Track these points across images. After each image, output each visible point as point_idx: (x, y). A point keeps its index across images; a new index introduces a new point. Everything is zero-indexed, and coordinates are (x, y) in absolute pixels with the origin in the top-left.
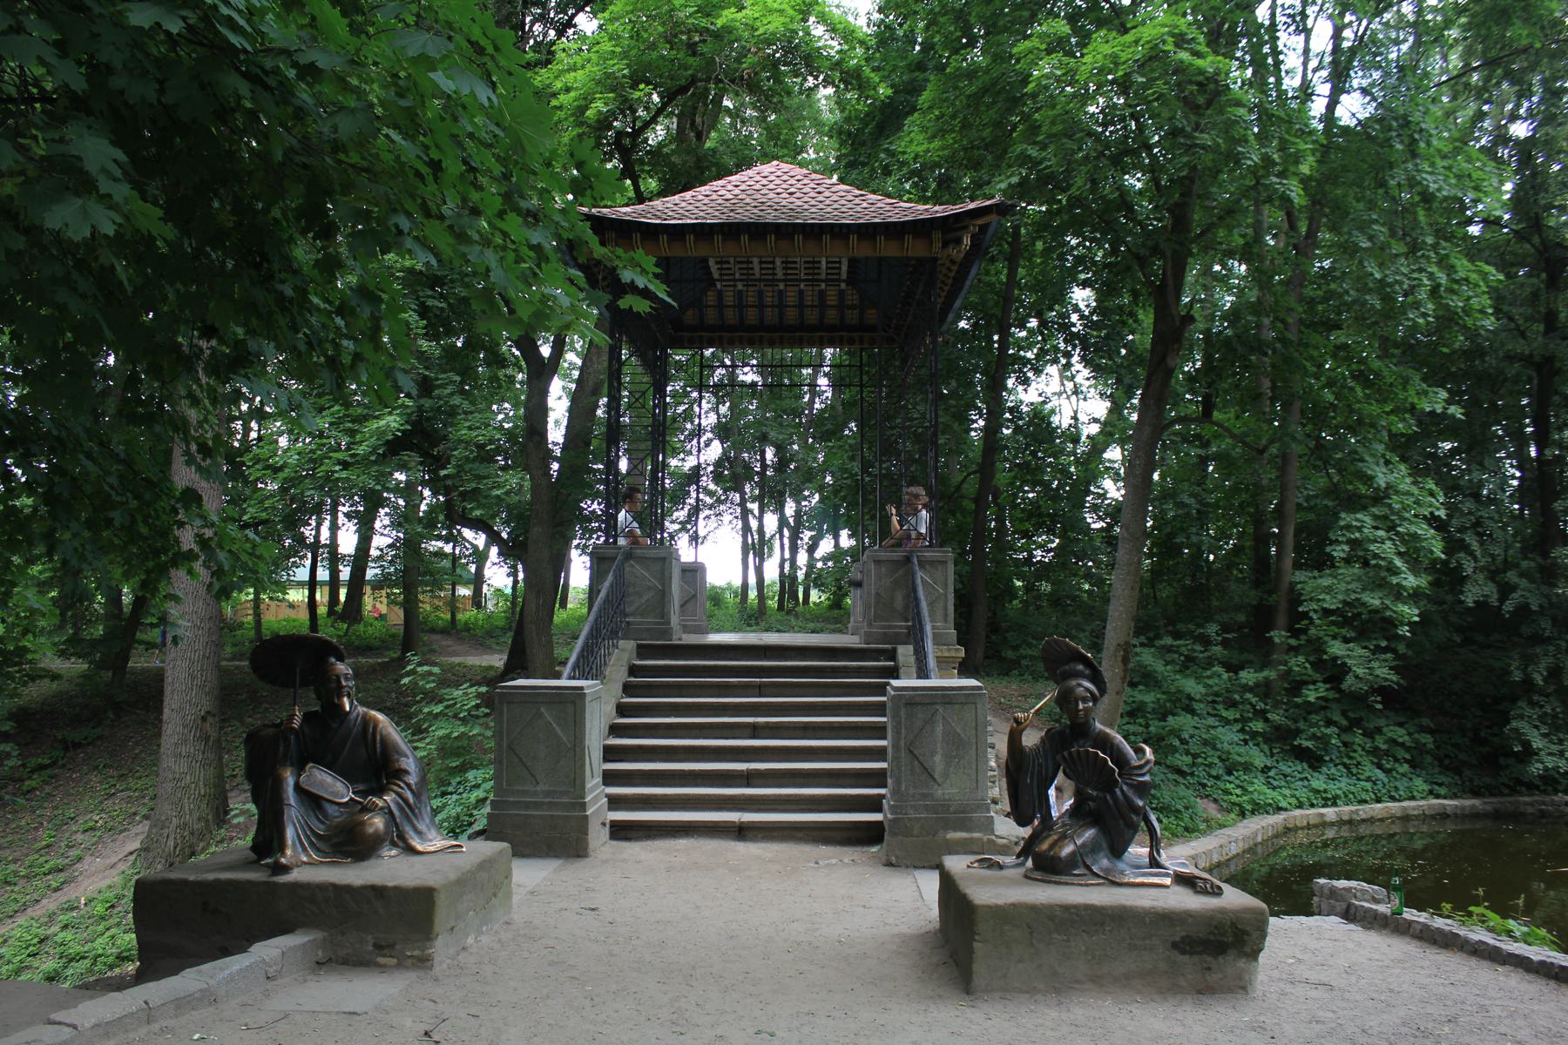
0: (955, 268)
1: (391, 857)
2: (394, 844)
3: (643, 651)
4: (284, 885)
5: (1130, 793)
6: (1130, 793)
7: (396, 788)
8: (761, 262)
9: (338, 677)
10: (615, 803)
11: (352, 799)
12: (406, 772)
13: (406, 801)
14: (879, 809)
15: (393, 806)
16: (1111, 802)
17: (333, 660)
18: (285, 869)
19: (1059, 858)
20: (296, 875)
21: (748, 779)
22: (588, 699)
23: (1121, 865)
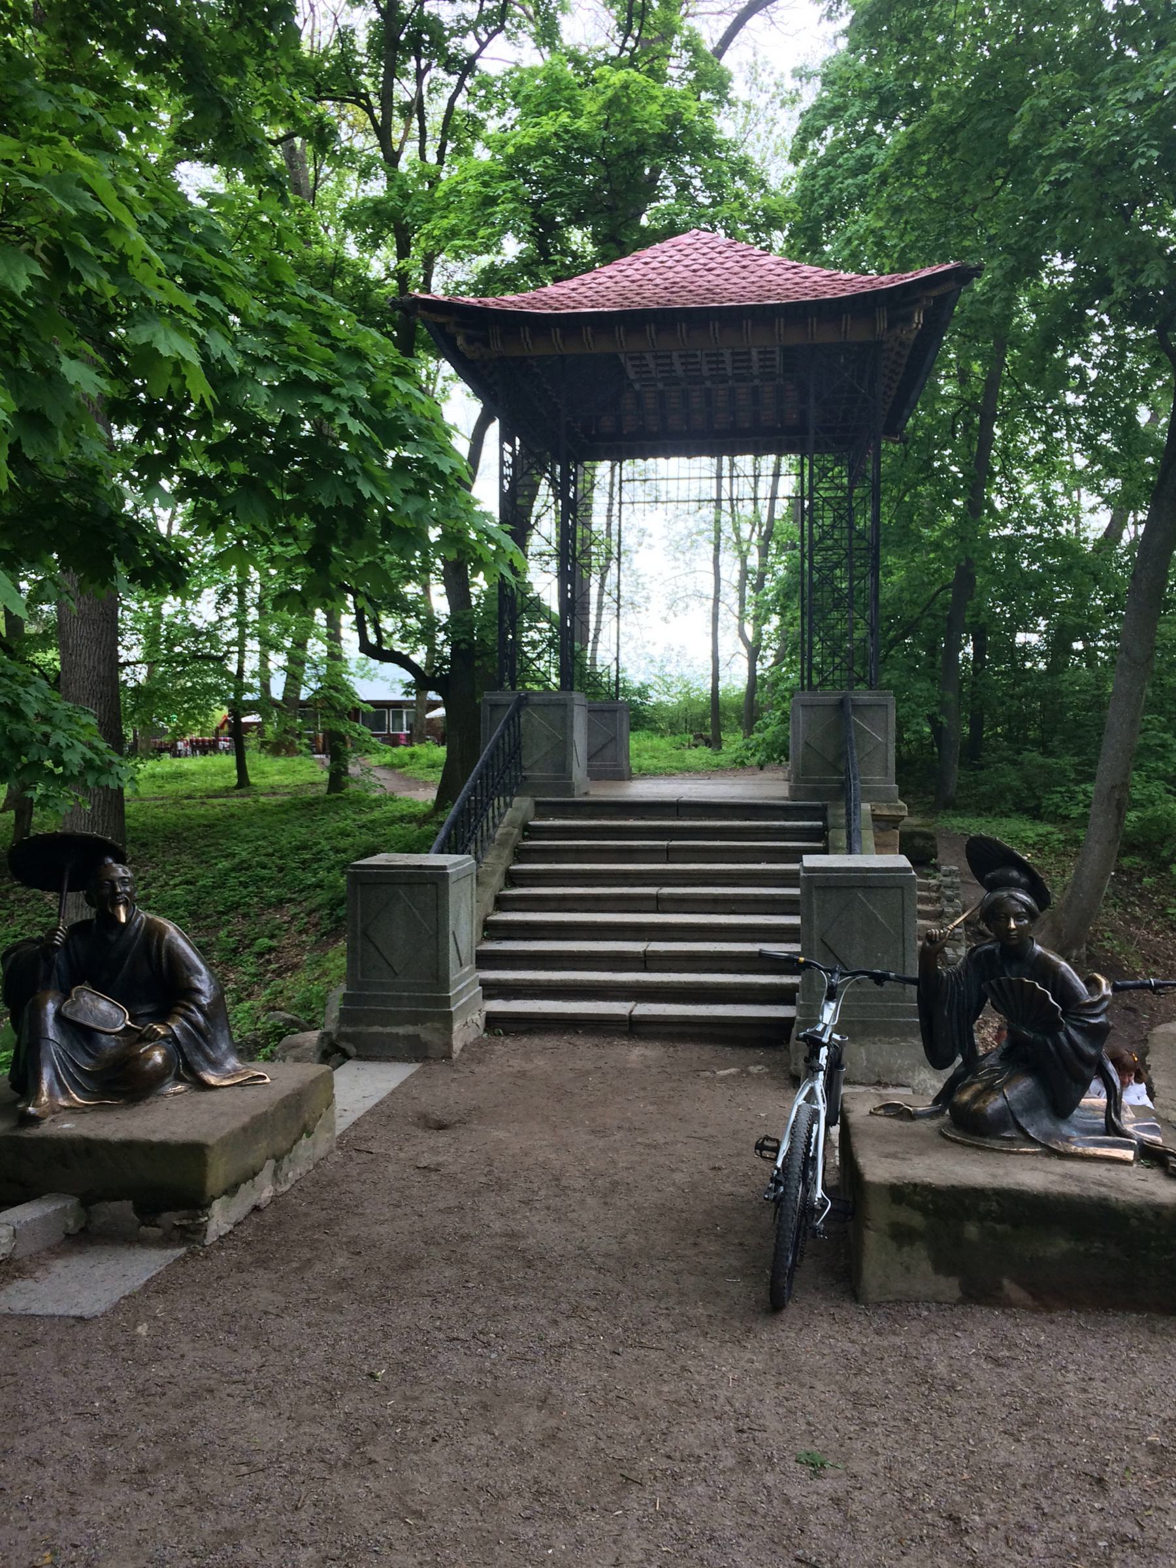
0: (907, 352)
1: (175, 1094)
2: (179, 1079)
3: (543, 809)
4: (31, 1140)
5: (1078, 1038)
6: (1078, 1038)
7: (182, 1011)
8: (733, 354)
9: (112, 882)
10: (492, 990)
11: (127, 1027)
12: (199, 991)
13: (195, 1025)
14: (791, 1002)
15: (177, 1032)
16: (1052, 1048)
17: (110, 861)
18: (35, 1120)
19: (984, 1116)
20: (47, 1129)
21: (645, 962)
22: (452, 879)
23: (1065, 1129)
